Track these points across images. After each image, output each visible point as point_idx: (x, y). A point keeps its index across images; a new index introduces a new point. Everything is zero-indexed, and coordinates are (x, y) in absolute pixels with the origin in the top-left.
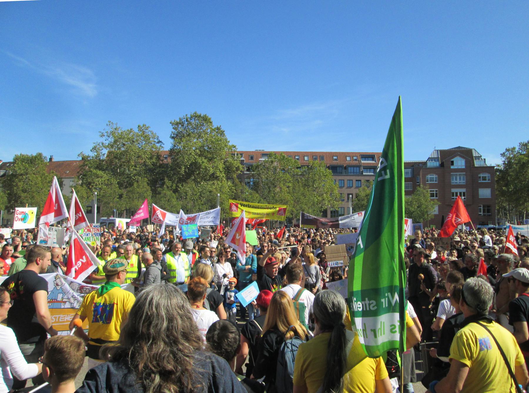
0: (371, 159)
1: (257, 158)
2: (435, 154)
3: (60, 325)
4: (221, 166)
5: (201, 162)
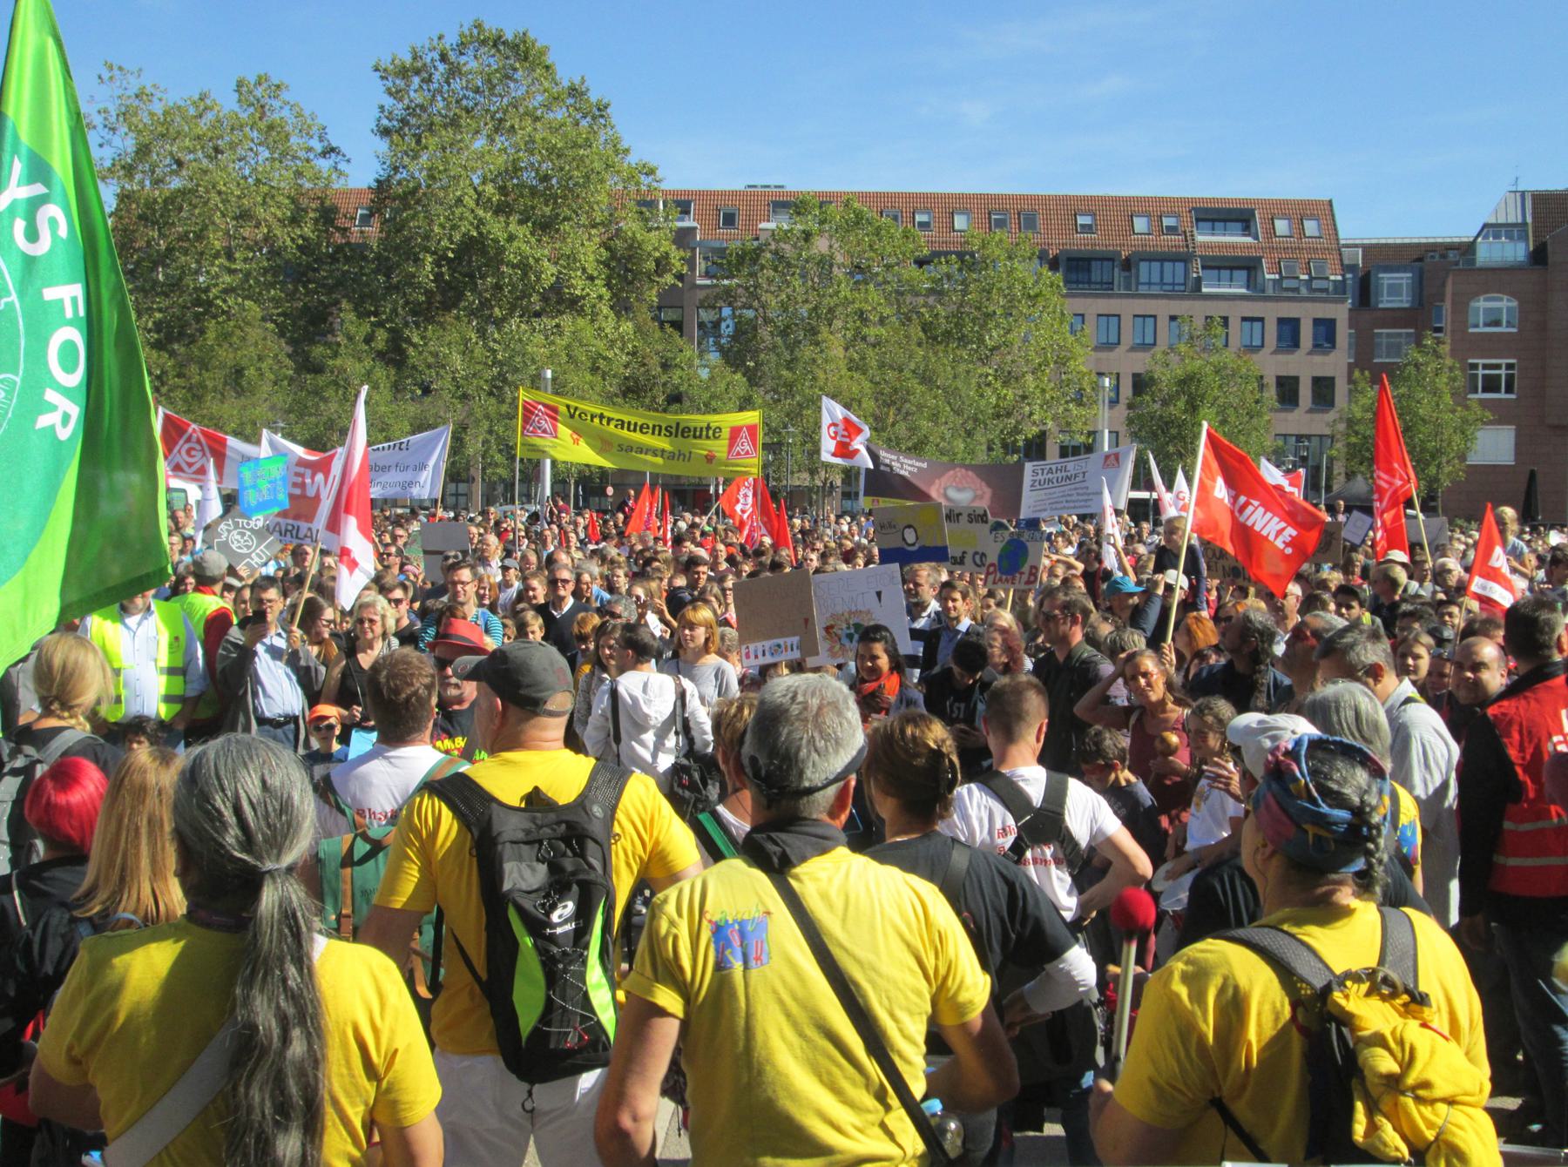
0: (1239, 225)
1: (751, 221)
2: (1511, 210)
3: (16, 907)
4: (590, 252)
5: (502, 237)
